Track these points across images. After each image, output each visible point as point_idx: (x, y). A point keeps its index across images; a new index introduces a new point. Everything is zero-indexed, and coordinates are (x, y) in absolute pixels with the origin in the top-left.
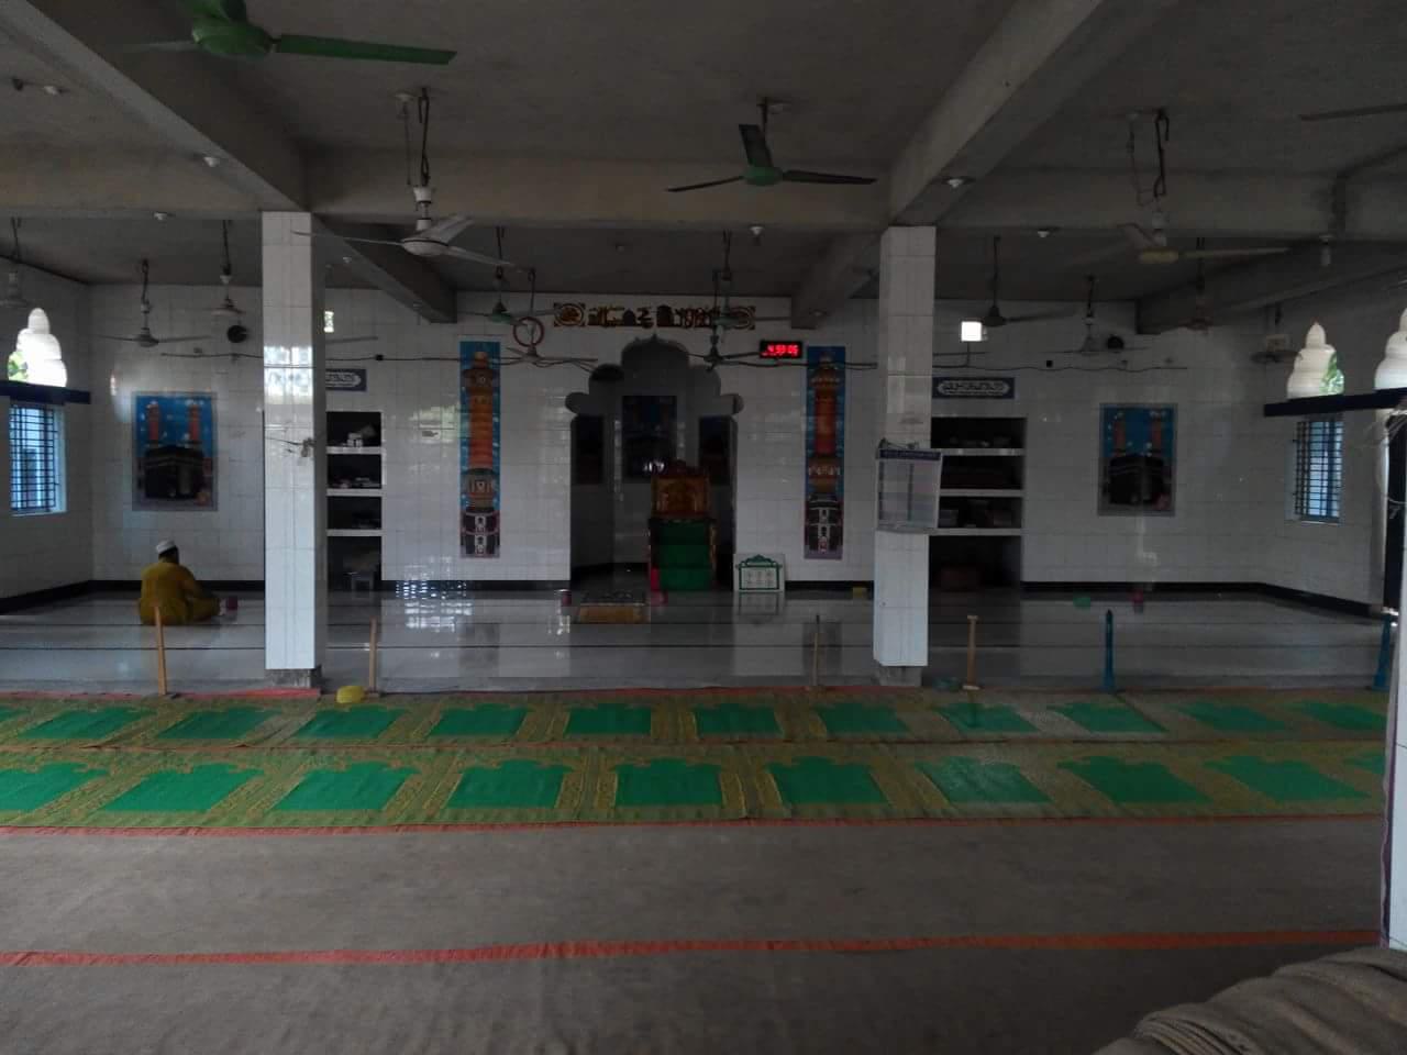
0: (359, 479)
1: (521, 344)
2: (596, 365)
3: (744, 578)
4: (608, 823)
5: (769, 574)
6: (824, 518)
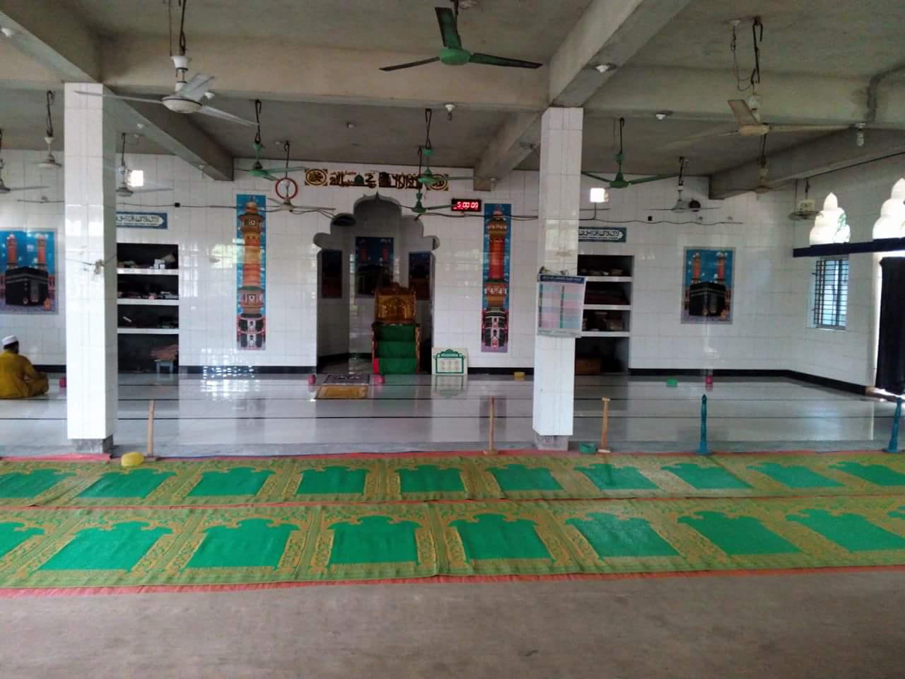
0: (163, 293)
1: (280, 196)
2: (336, 213)
3: (439, 365)
4: (321, 583)
5: (456, 362)
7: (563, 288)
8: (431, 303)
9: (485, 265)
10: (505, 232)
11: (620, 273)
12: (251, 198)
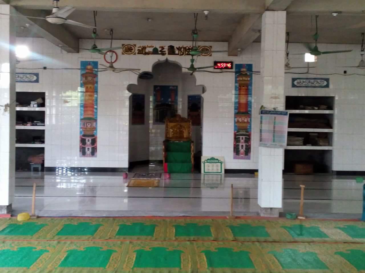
0: (35, 122)
2: (141, 72)
3: (206, 167)
6: (242, 141)
7: (275, 118)
8: (201, 127)
9: (235, 103)
10: (249, 82)
11: (325, 108)
12: (89, 63)
